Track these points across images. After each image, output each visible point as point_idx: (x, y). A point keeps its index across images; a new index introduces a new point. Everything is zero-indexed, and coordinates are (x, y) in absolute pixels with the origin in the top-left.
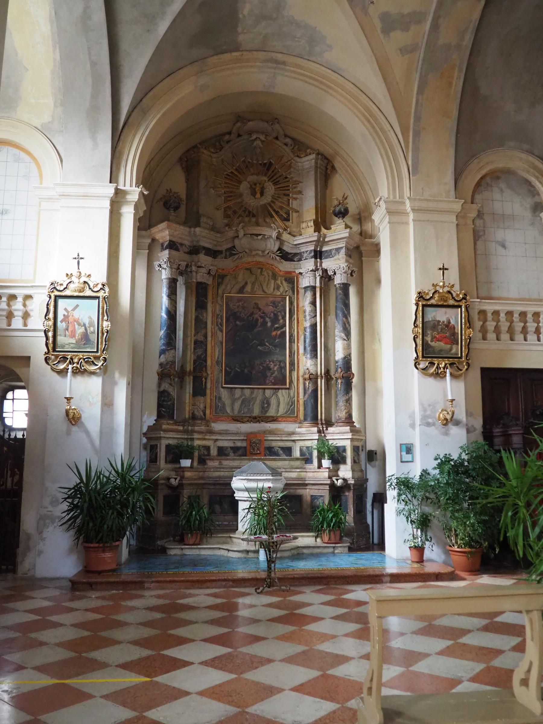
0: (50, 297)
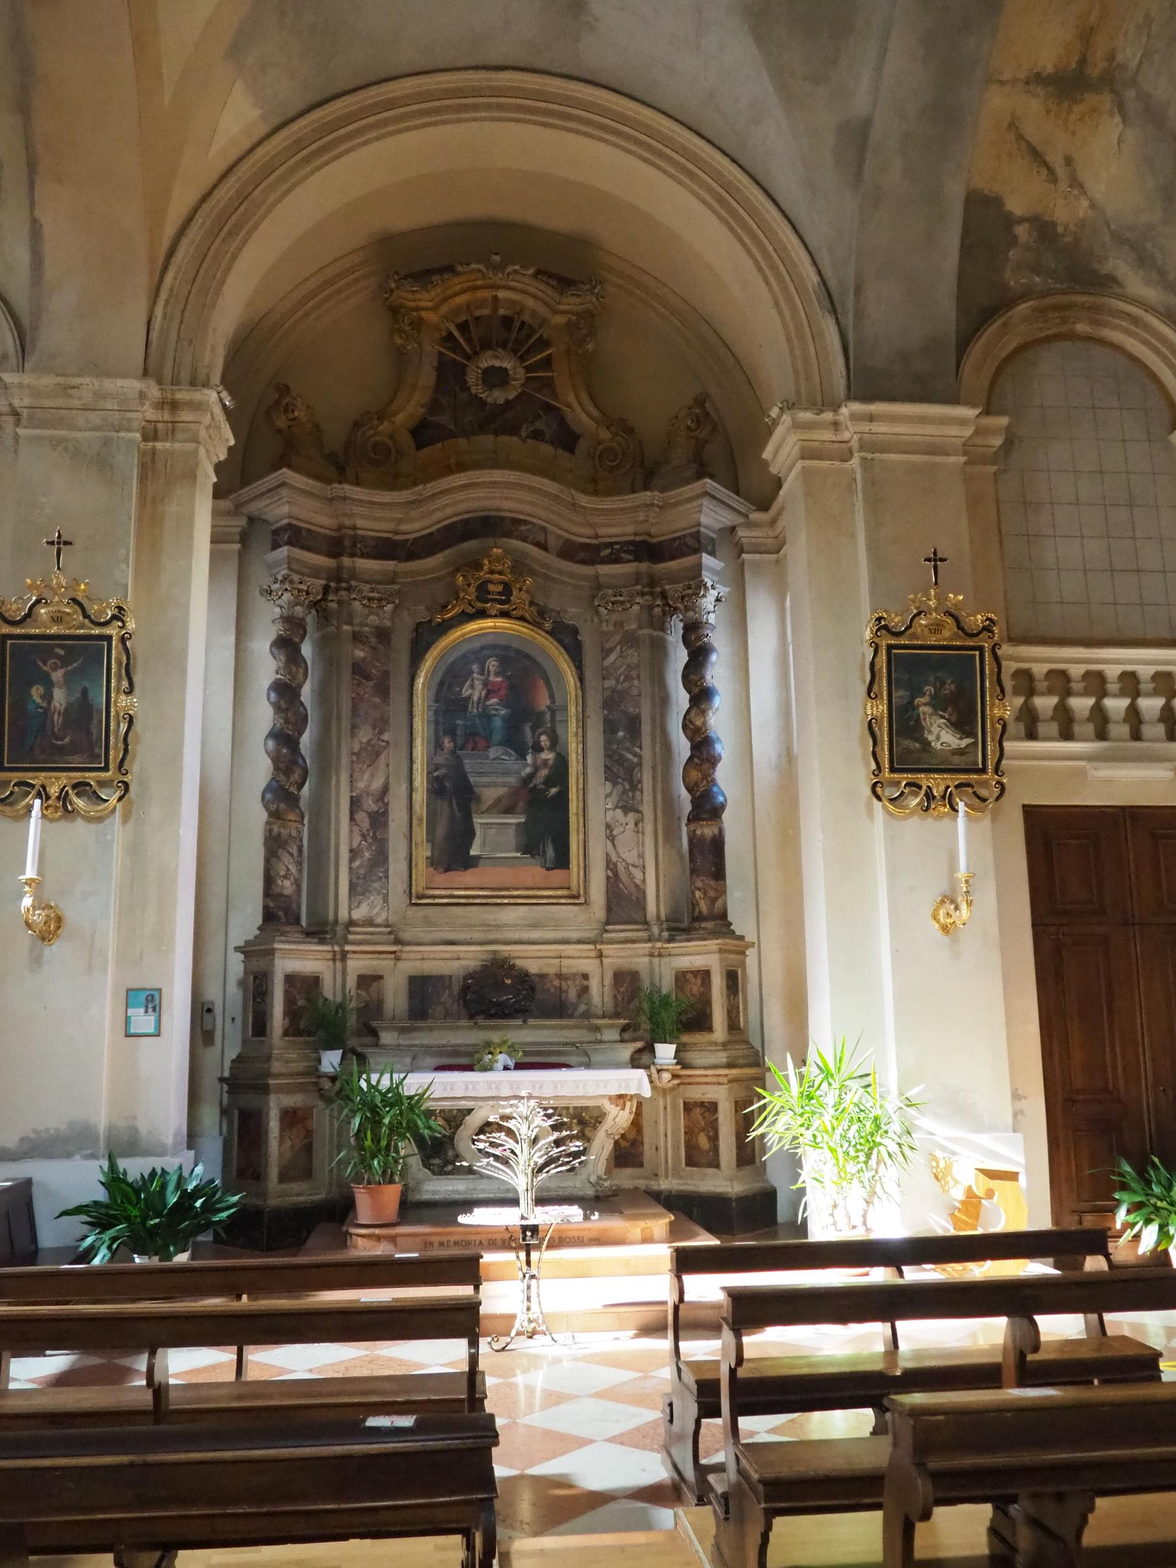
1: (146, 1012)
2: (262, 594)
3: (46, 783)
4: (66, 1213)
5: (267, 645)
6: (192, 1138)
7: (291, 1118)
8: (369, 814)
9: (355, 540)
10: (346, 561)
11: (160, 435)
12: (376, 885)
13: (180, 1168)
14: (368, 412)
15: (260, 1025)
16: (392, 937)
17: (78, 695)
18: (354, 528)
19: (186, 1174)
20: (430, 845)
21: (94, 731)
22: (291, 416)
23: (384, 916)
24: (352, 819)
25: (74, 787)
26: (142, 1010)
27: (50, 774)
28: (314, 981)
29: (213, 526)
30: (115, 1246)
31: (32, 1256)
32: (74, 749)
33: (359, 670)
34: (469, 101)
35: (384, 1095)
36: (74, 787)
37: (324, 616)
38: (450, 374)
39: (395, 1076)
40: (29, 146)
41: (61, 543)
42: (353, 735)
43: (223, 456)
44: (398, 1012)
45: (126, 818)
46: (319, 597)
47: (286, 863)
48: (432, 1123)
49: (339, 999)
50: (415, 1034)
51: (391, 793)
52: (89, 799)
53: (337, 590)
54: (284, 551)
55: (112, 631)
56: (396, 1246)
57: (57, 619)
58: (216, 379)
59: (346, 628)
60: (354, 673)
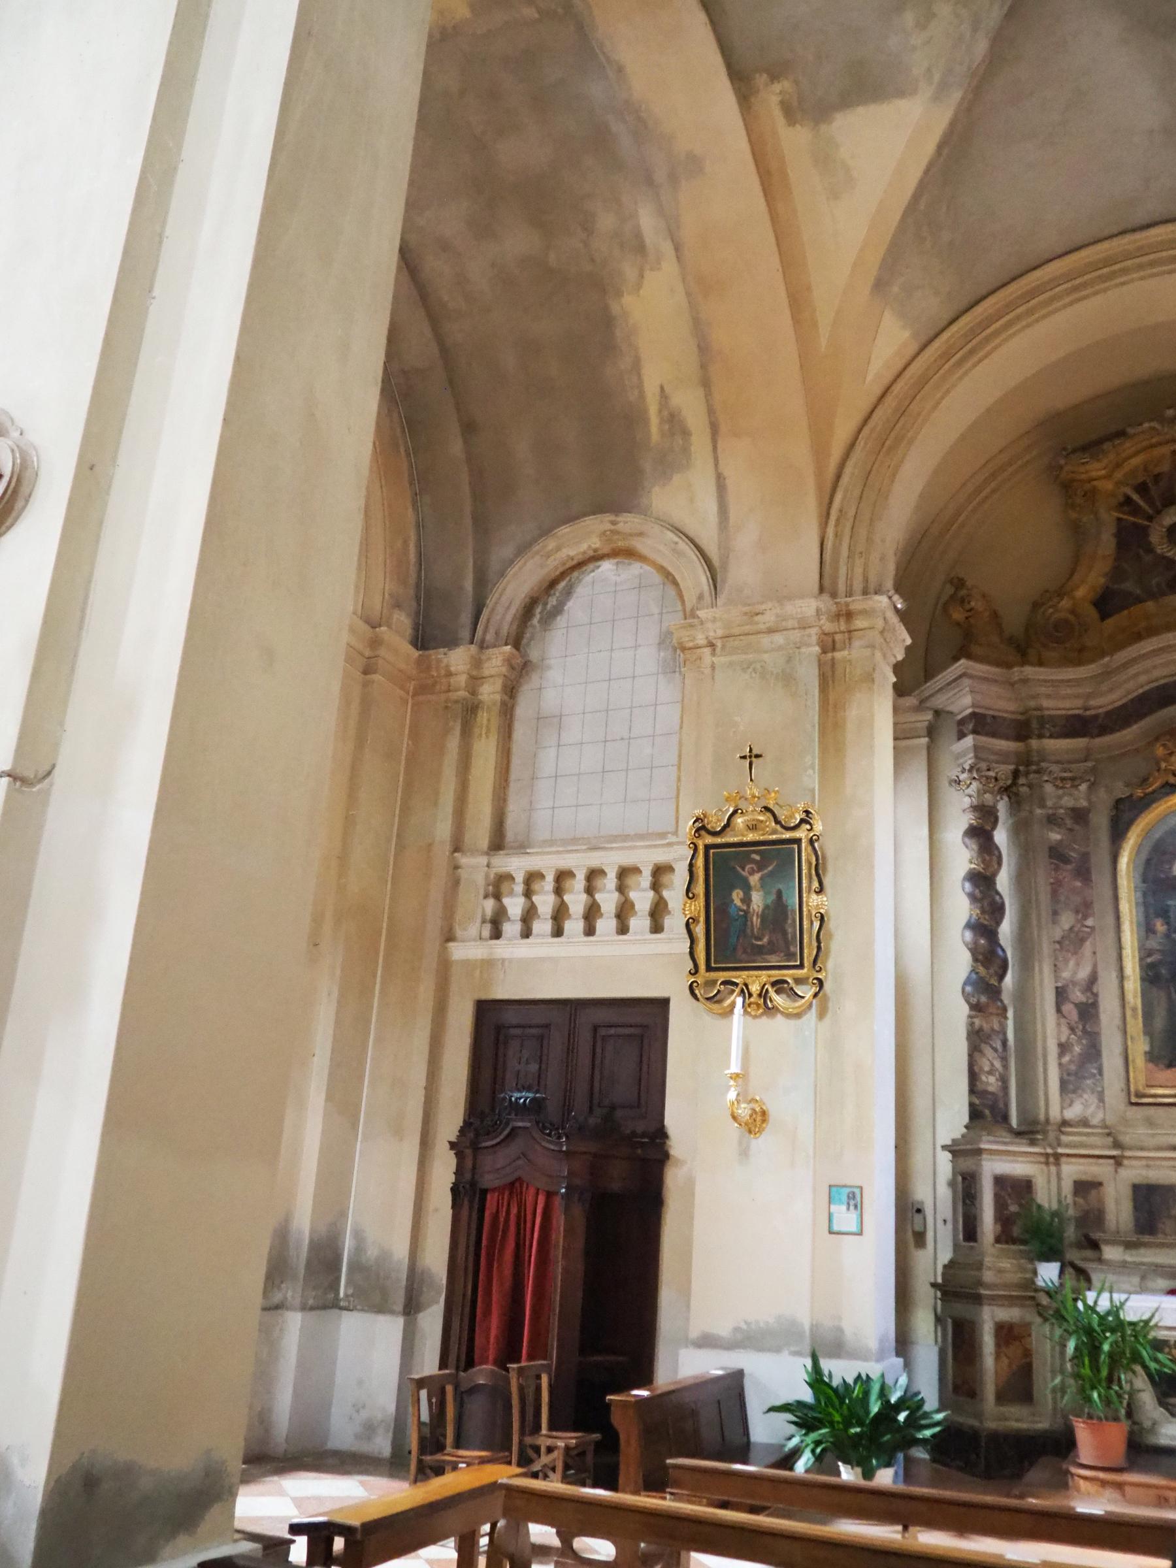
0: (696, 849)
1: (848, 1209)
2: (950, 784)
3: (749, 981)
4: (773, 1409)
5: (961, 833)
6: (903, 1344)
7: (1007, 1334)
8: (1076, 1005)
9: (1042, 721)
10: (1034, 743)
11: (838, 646)
12: (1088, 1082)
13: (883, 1376)
14: (1047, 591)
15: (970, 1231)
16: (1110, 1139)
17: (773, 897)
18: (1039, 709)
19: (889, 1381)
20: (1148, 1039)
21: (790, 930)
22: (968, 607)
23: (1100, 1115)
24: (1059, 1010)
25: (773, 984)
26: (844, 1207)
27: (752, 973)
28: (1023, 1187)
29: (895, 724)
30: (818, 1450)
31: (743, 1452)
32: (772, 949)
33: (1057, 854)
34: (1078, 281)
35: (1103, 1318)
36: (773, 984)
37: (1016, 803)
38: (1131, 539)
39: (1116, 1296)
40: (711, 411)
41: (752, 757)
42: (1054, 922)
43: (900, 656)
44: (1122, 1227)
45: (822, 1015)
46: (1009, 782)
47: (989, 1059)
48: (1160, 1356)
49: (1055, 1206)
50: (1142, 1251)
51: (1100, 981)
52: (788, 996)
53: (1027, 773)
54: (969, 741)
55: (801, 834)
56: (1124, 1496)
57: (753, 827)
58: (889, 584)
59: (1038, 811)
60: (1050, 857)
